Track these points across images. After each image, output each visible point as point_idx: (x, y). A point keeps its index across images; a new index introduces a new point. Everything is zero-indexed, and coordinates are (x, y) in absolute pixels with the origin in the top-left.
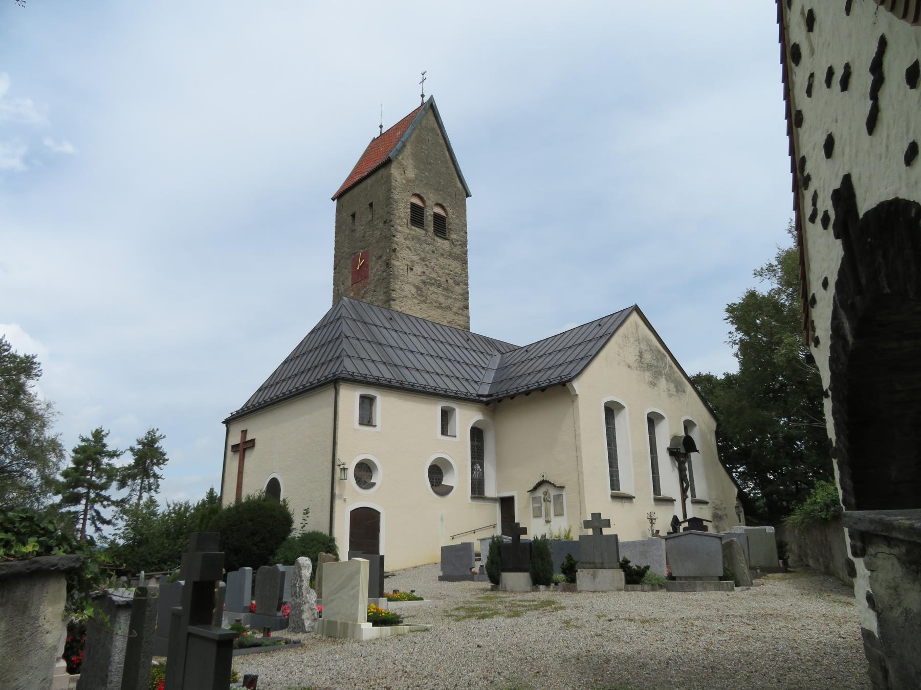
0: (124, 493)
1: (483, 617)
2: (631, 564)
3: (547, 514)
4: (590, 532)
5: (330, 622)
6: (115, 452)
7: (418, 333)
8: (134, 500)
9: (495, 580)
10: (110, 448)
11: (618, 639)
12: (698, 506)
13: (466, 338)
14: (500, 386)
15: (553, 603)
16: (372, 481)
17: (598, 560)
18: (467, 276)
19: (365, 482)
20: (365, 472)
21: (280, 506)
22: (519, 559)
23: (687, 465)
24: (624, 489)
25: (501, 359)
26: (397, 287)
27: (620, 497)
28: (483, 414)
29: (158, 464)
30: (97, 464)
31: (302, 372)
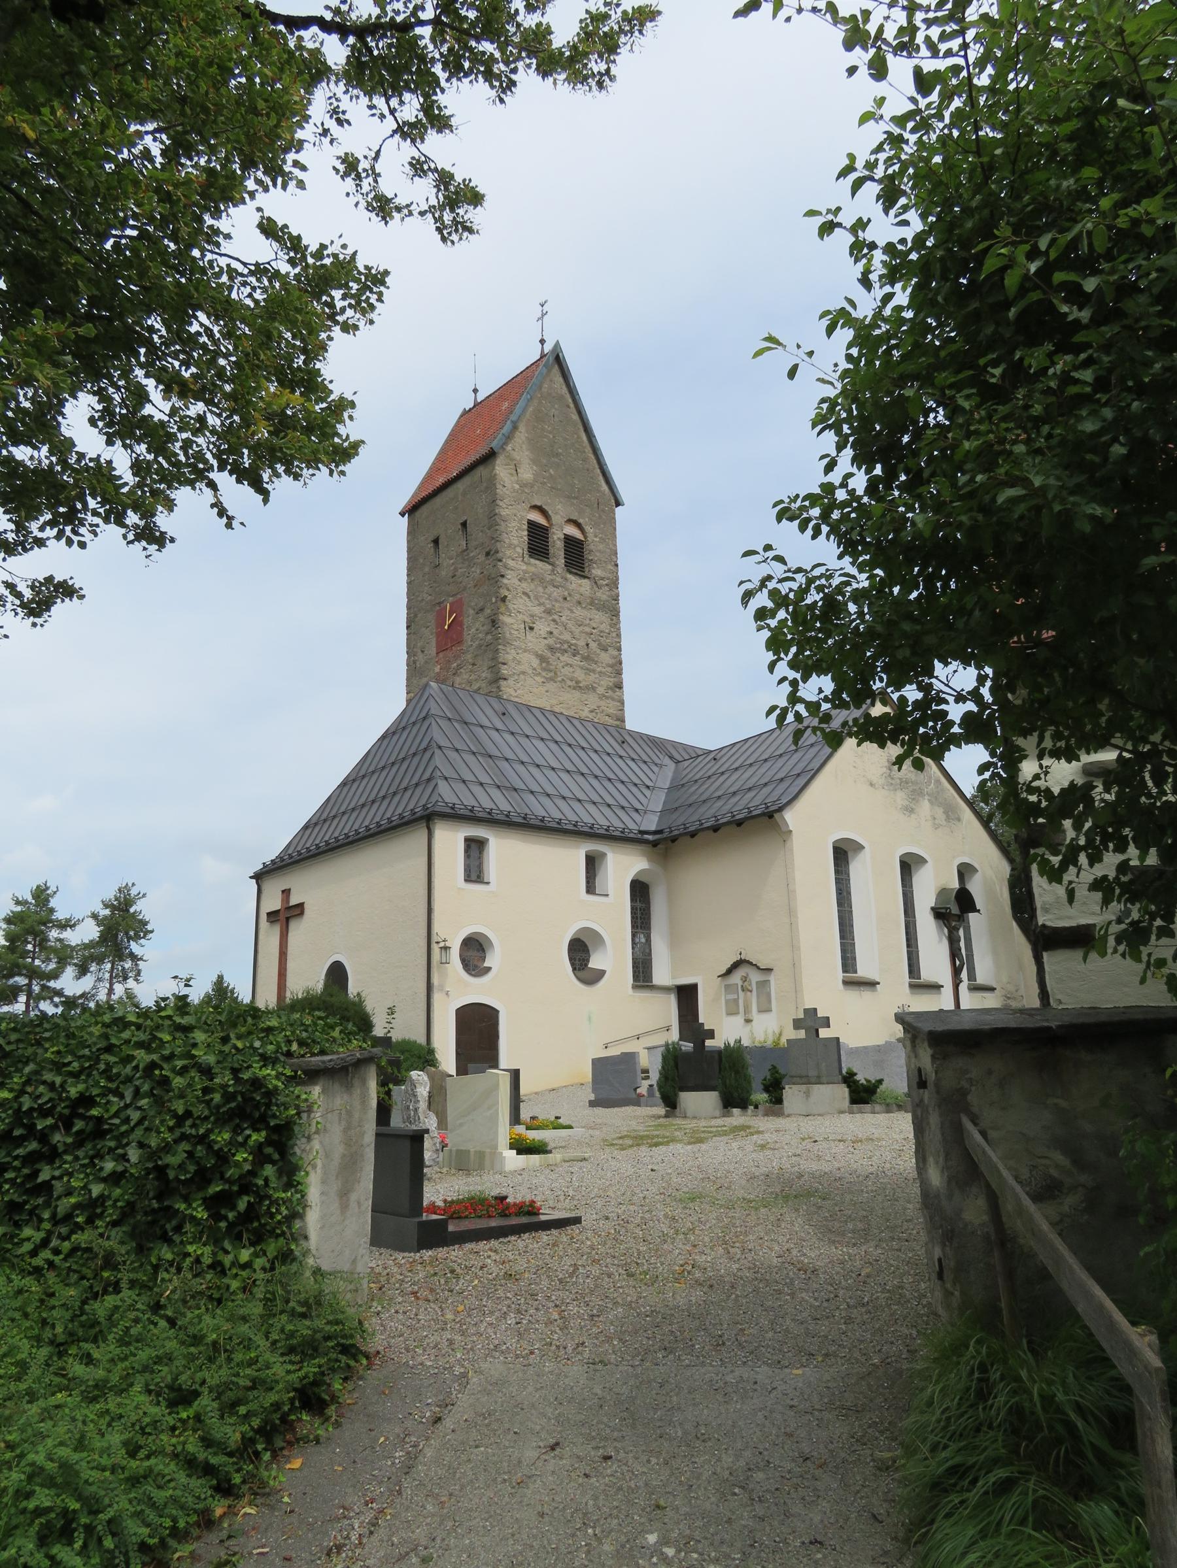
1: (656, 1145)
2: (857, 1078)
3: (747, 1010)
4: (802, 1034)
6: (68, 920)
7: (546, 736)
8: (102, 996)
9: (671, 1103)
10: (60, 915)
12: (979, 995)
13: (620, 739)
14: (674, 816)
15: (749, 1127)
16: (486, 964)
17: (813, 1073)
18: (619, 636)
19: (476, 967)
20: (475, 951)
21: (354, 1004)
22: (702, 1071)
23: (961, 932)
24: (864, 970)
25: (676, 772)
26: (510, 657)
28: (650, 860)
29: (137, 938)
30: (42, 942)
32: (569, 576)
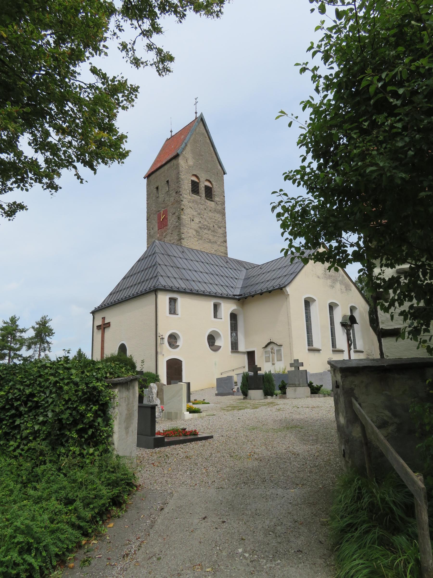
0: (30, 353)
1: (240, 409)
2: (313, 384)
3: (273, 360)
4: (293, 369)
5: (168, 413)
6: (23, 329)
9: (245, 394)
10: (20, 327)
11: (299, 414)
13: (226, 261)
14: (246, 289)
16: (177, 344)
17: (297, 383)
18: (225, 223)
19: (173, 345)
20: (173, 339)
21: (129, 359)
22: (256, 382)
23: (351, 331)
24: (316, 345)
25: (247, 273)
26: (185, 231)
27: (312, 350)
28: (237, 306)
29: (49, 335)
30: (14, 337)
31: (135, 285)
32: (207, 201)
